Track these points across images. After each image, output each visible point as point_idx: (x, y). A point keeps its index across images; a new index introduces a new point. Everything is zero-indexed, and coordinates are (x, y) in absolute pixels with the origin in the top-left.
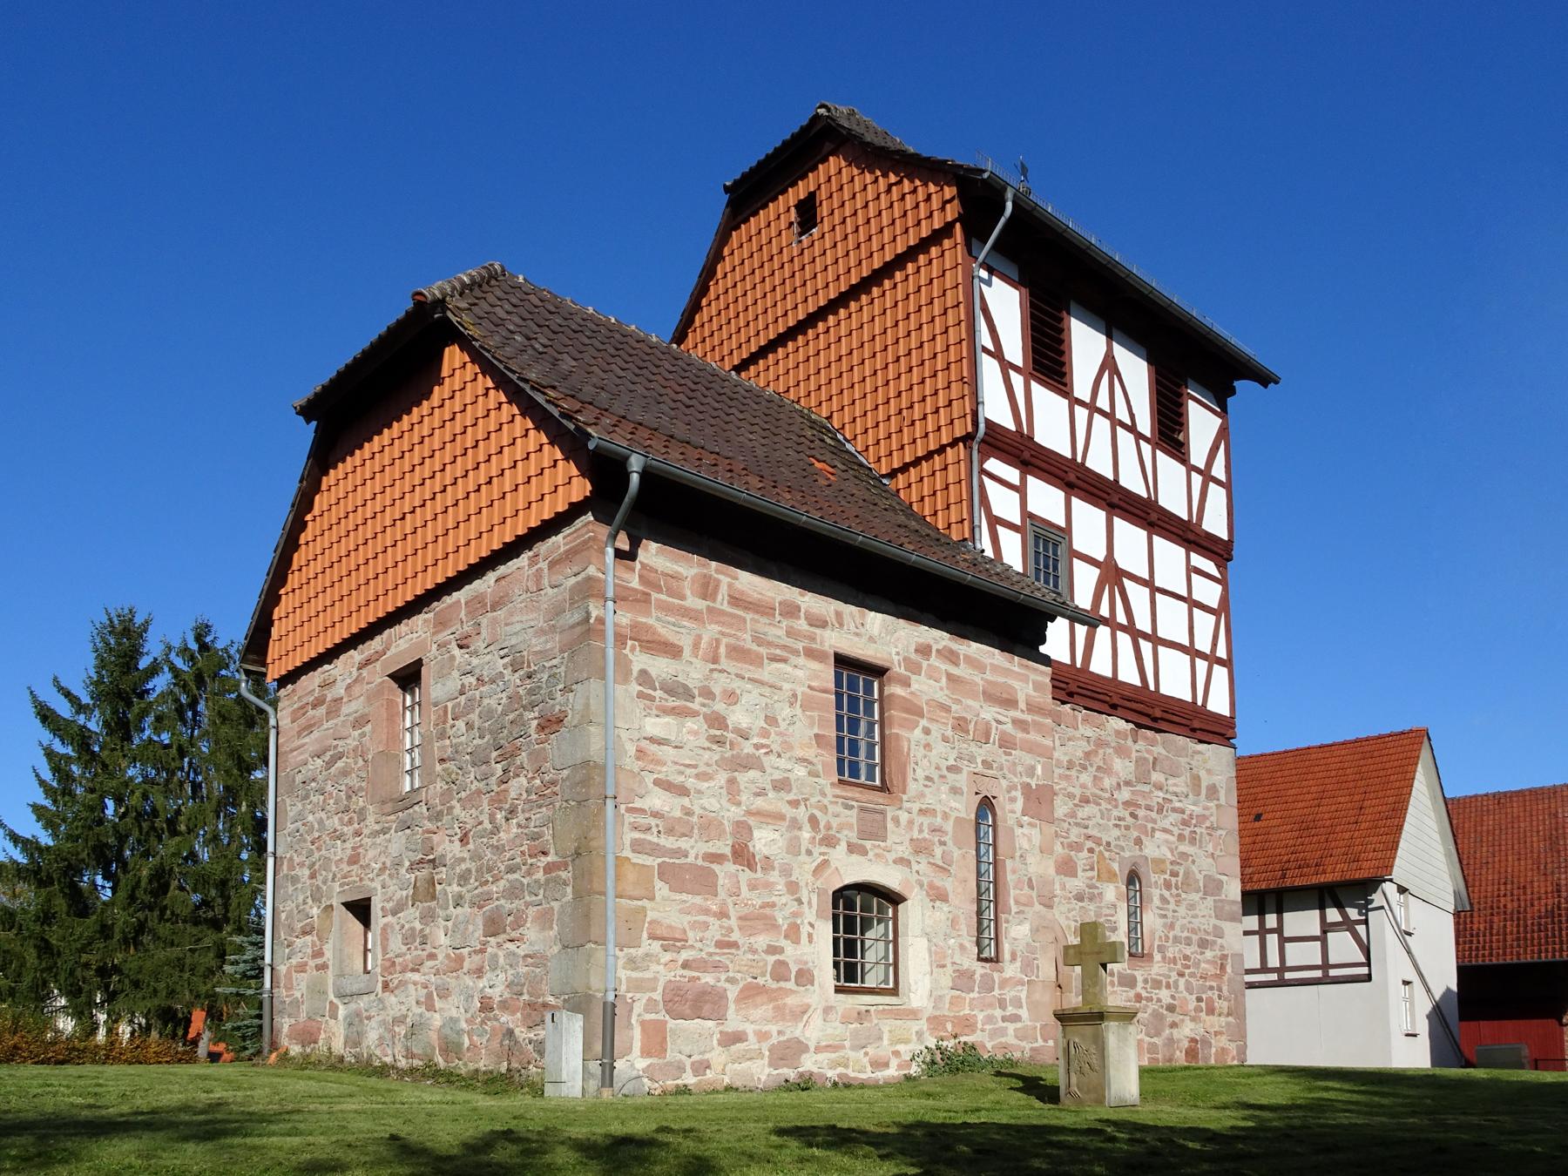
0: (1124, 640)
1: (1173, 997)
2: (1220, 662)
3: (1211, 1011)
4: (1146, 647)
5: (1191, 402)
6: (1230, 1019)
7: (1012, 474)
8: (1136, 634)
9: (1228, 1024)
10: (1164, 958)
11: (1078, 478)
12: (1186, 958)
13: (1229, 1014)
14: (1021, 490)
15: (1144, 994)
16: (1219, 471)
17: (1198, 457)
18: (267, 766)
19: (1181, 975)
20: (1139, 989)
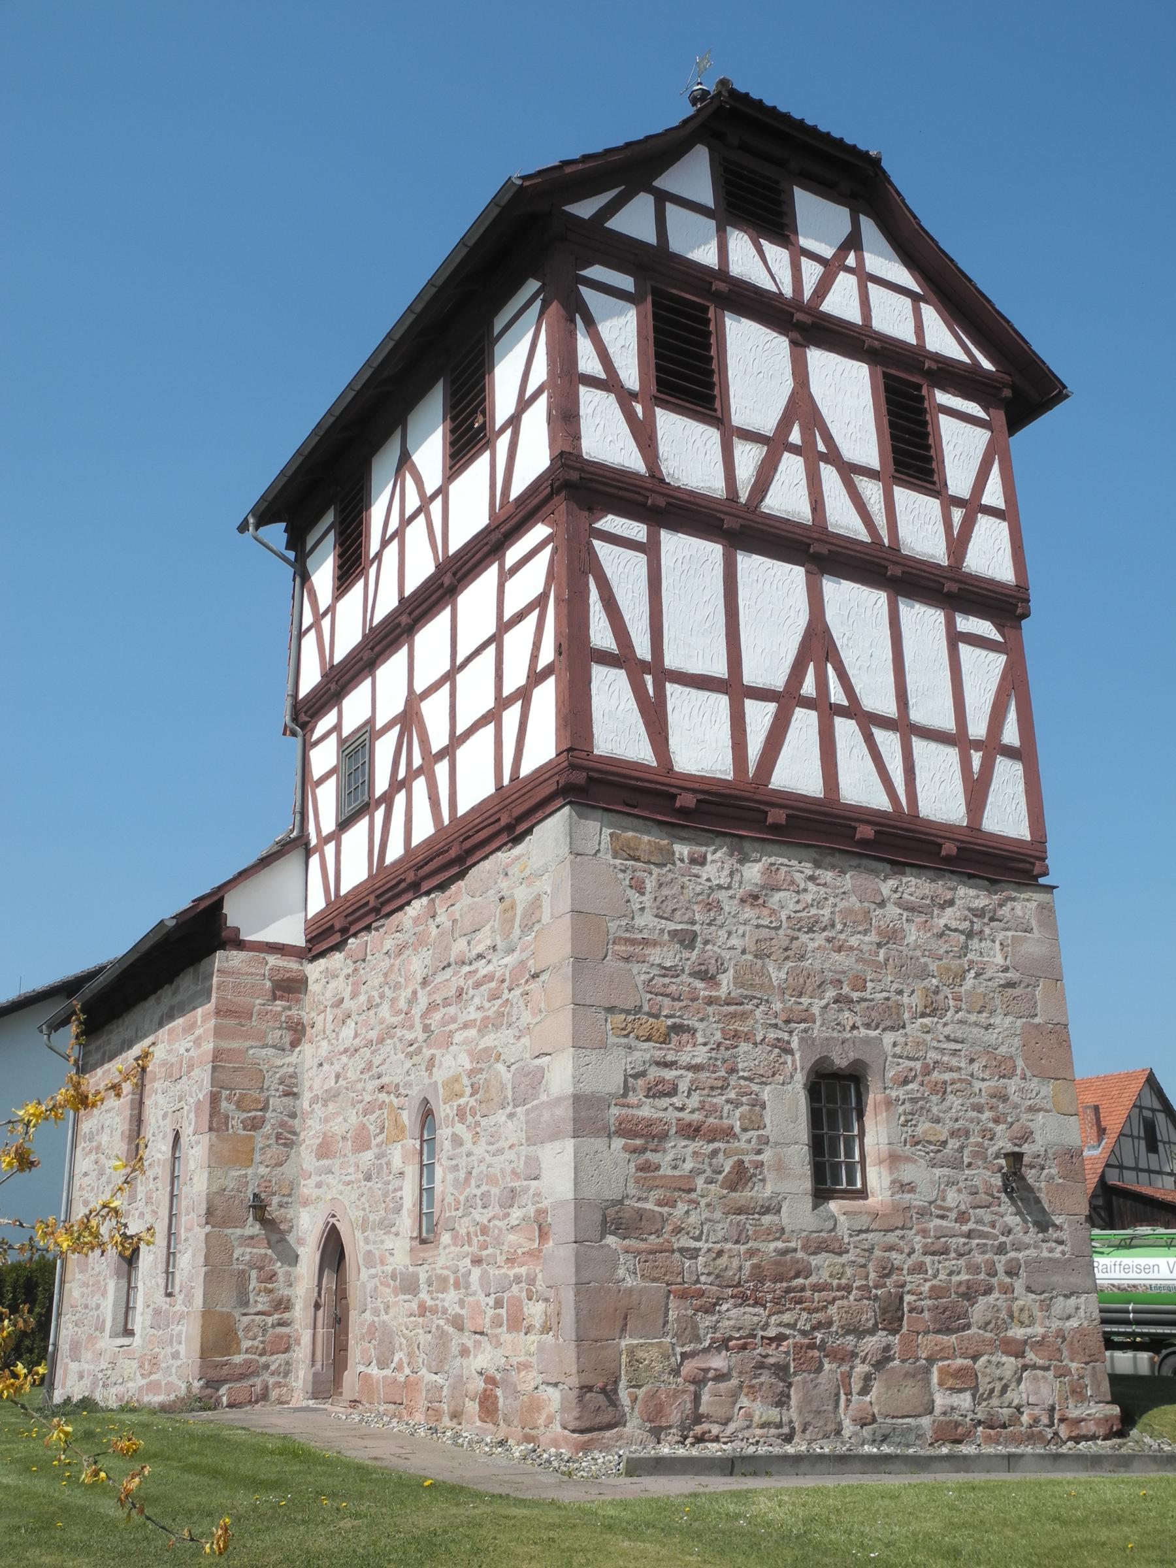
0: (846, 729)
1: (461, 1303)
2: (1011, 753)
3: (516, 1322)
4: (888, 741)
5: (943, 419)
6: (549, 1338)
7: (637, 530)
8: (868, 721)
9: (541, 1348)
10: (455, 1238)
11: (372, 649)
12: (484, 1231)
13: (546, 1329)
14: (651, 550)
15: (429, 1303)
16: (993, 495)
17: (959, 480)
18: (748, 1491)
19: (477, 1261)
20: (424, 1295)
